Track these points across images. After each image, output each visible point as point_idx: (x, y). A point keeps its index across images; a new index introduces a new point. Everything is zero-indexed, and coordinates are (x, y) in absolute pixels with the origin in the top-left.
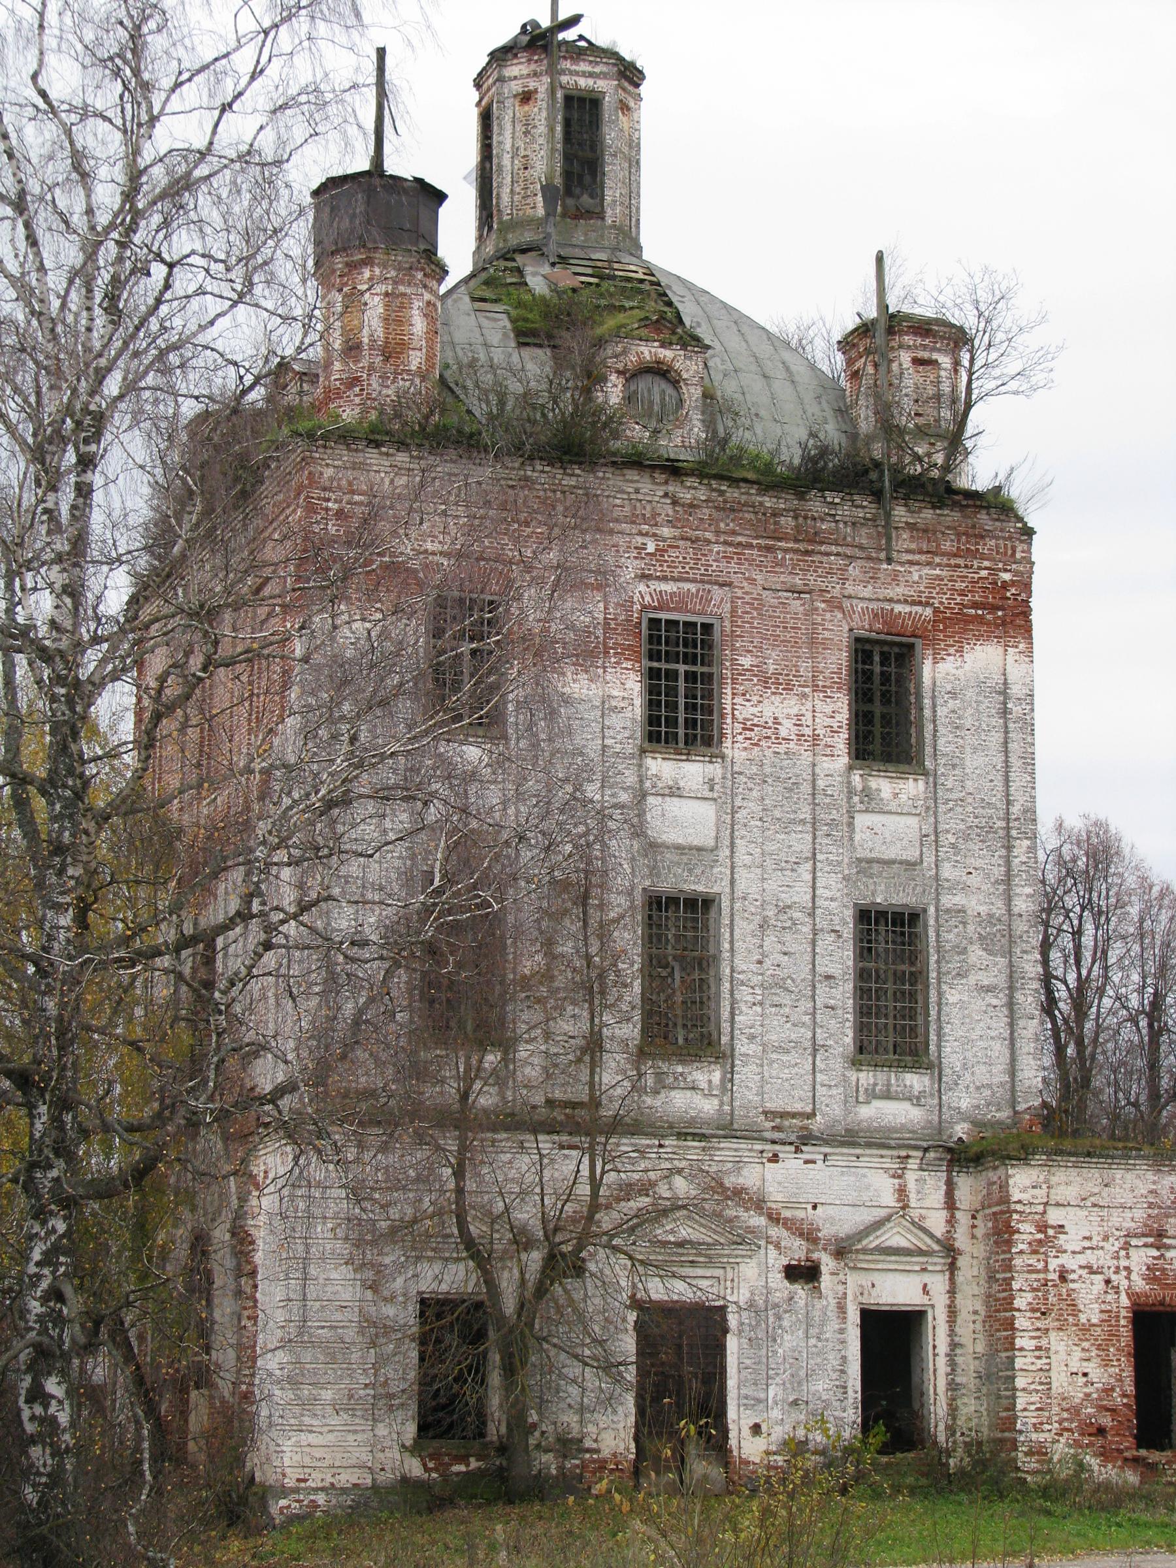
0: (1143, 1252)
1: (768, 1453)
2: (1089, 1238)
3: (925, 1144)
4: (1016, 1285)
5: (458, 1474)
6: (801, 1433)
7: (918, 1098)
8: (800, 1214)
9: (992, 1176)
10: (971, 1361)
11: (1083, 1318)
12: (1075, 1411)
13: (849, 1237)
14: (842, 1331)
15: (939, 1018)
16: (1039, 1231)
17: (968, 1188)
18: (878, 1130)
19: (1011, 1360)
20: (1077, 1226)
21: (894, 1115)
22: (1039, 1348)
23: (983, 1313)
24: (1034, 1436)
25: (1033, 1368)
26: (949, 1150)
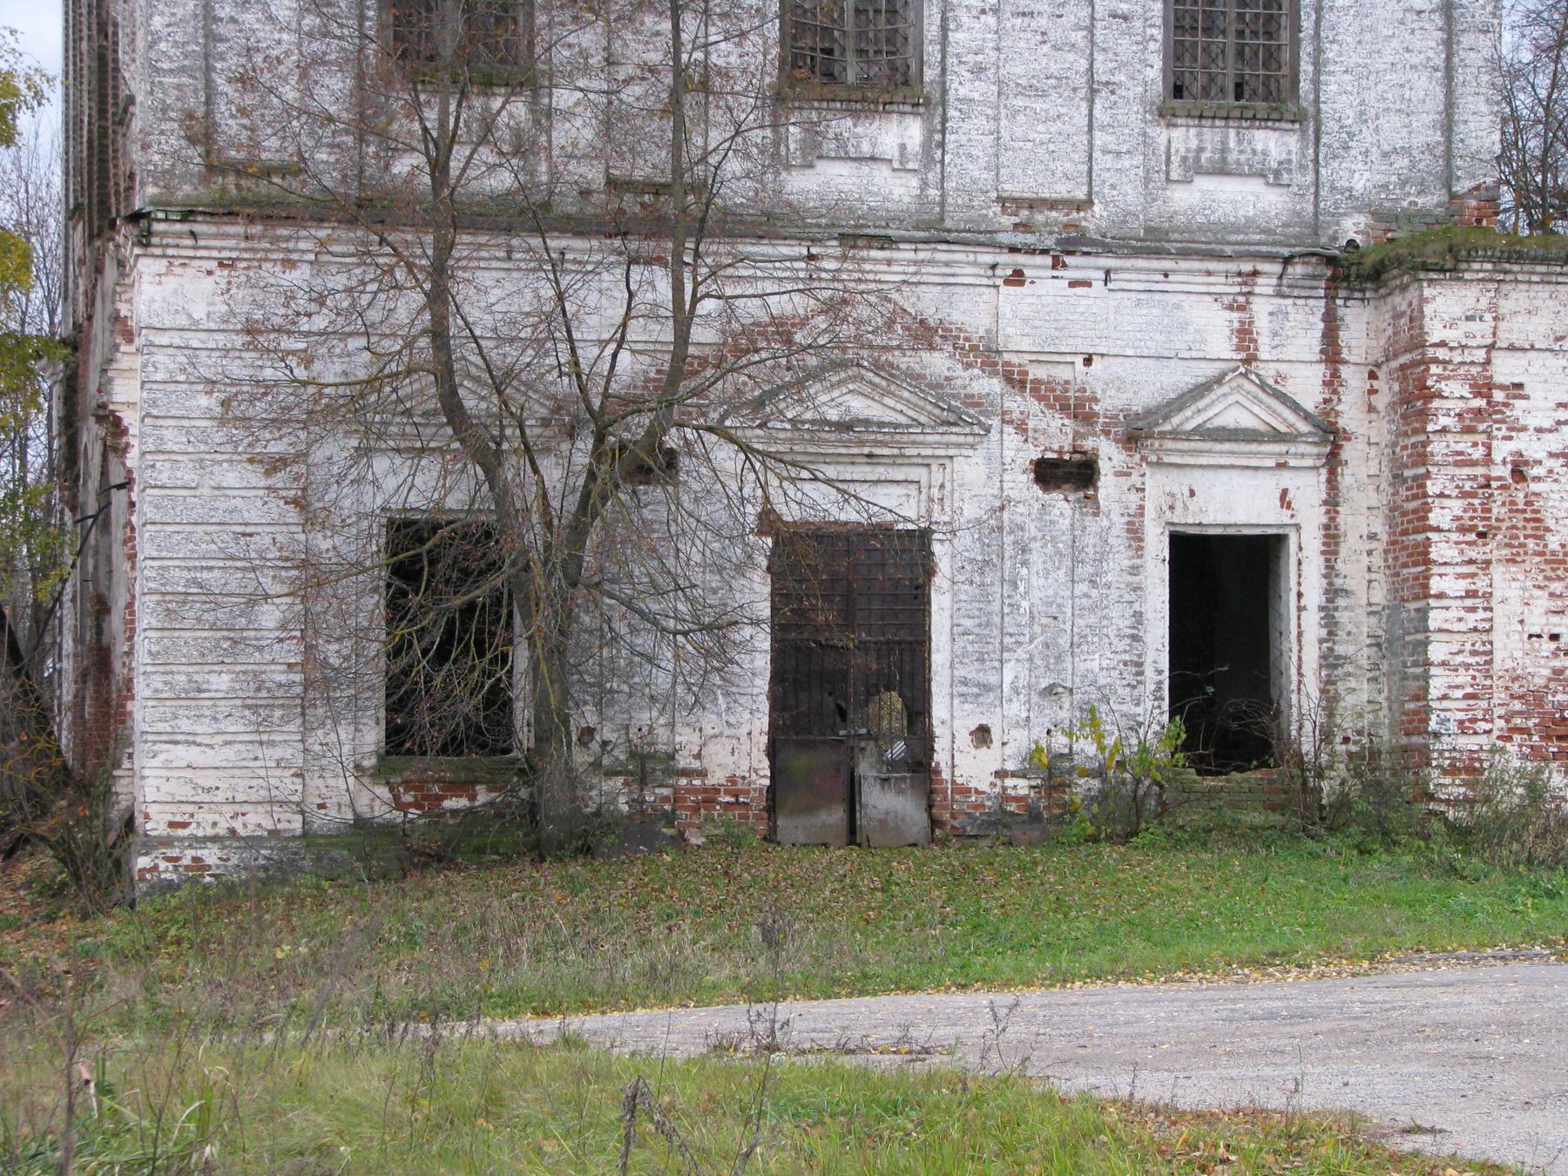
1: (1001, 774)
3: (1286, 252)
4: (1432, 488)
5: (454, 812)
6: (1060, 742)
8: (1063, 373)
9: (1400, 301)
10: (1364, 618)
12: (1535, 699)
13: (1149, 412)
14: (1135, 570)
15: (1317, 34)
16: (1478, 394)
17: (1362, 327)
18: (1209, 227)
19: (1423, 614)
21: (1234, 202)
22: (1472, 594)
23: (1385, 537)
25: (1462, 627)
26: (1331, 261)
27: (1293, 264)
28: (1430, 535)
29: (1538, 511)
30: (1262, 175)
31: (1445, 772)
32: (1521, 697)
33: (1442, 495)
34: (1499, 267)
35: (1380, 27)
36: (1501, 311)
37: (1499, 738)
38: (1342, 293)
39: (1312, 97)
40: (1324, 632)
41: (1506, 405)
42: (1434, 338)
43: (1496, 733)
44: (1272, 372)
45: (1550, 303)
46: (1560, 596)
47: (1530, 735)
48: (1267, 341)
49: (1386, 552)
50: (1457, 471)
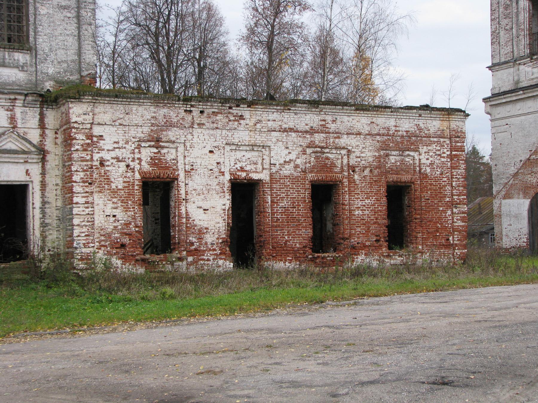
0: (148, 150)
2: (117, 143)
3: (26, 92)
4: (74, 168)
7: (22, 67)
9: (63, 109)
10: (54, 211)
11: (113, 186)
15: (35, 22)
16: (88, 139)
17: (52, 118)
19: (71, 209)
20: (110, 136)
21: (8, 76)
22: (87, 203)
23: (61, 185)
24: (84, 250)
26: (41, 96)
27: (28, 96)
28: (73, 184)
29: (108, 176)
30: (17, 67)
31: (79, 260)
32: (104, 235)
33: (77, 171)
34: (94, 98)
35: (56, 22)
36: (95, 112)
37: (97, 248)
38: (45, 106)
39: (34, 43)
40: (41, 216)
41: (97, 142)
42: (73, 120)
43: (96, 247)
44: (22, 131)
45: (111, 110)
46: (116, 203)
47: (107, 247)
48: (20, 121)
49: (61, 189)
50: (82, 163)
